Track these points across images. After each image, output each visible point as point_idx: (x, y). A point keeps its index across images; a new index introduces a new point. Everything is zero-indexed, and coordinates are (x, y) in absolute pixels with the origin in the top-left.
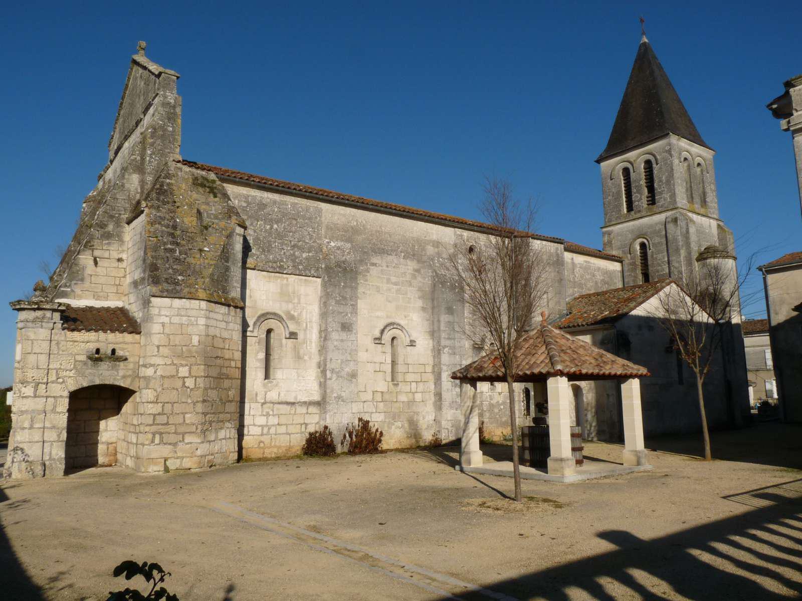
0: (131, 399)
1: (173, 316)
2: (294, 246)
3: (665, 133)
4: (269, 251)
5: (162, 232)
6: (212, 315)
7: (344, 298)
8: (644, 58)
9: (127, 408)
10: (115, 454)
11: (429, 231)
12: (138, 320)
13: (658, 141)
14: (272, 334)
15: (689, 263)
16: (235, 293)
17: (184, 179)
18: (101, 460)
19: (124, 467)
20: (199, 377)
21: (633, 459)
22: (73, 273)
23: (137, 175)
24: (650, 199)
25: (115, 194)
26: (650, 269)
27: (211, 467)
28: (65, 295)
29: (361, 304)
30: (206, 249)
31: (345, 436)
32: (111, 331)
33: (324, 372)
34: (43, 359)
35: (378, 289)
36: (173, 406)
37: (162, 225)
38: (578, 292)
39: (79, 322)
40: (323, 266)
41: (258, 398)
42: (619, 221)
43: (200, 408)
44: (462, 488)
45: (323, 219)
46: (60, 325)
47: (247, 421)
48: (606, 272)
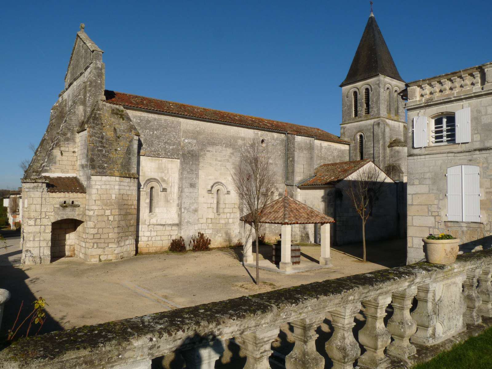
0: (81, 225)
1: (102, 185)
2: (166, 143)
3: (377, 74)
5: (96, 141)
6: (122, 183)
7: (192, 170)
8: (371, 25)
9: (80, 228)
10: (74, 250)
11: (240, 132)
12: (85, 186)
13: (373, 78)
14: (154, 189)
15: (384, 149)
16: (134, 171)
17: (107, 110)
18: (67, 253)
19: (78, 257)
20: (115, 215)
21: (324, 262)
22: (51, 159)
23: (82, 107)
24: (367, 110)
25: (71, 117)
26: (364, 150)
27: (122, 259)
28: (46, 171)
29: (201, 173)
30: (119, 149)
31: (191, 242)
32: (71, 192)
33: (180, 209)
34: (38, 207)
35: (210, 164)
36: (103, 230)
37: (96, 137)
38: (323, 162)
39: (55, 187)
40: (181, 153)
41: (146, 222)
42: (350, 122)
43: (116, 230)
44: (237, 276)
45: (182, 127)
46: (46, 190)
47: (141, 234)
48: (340, 151)
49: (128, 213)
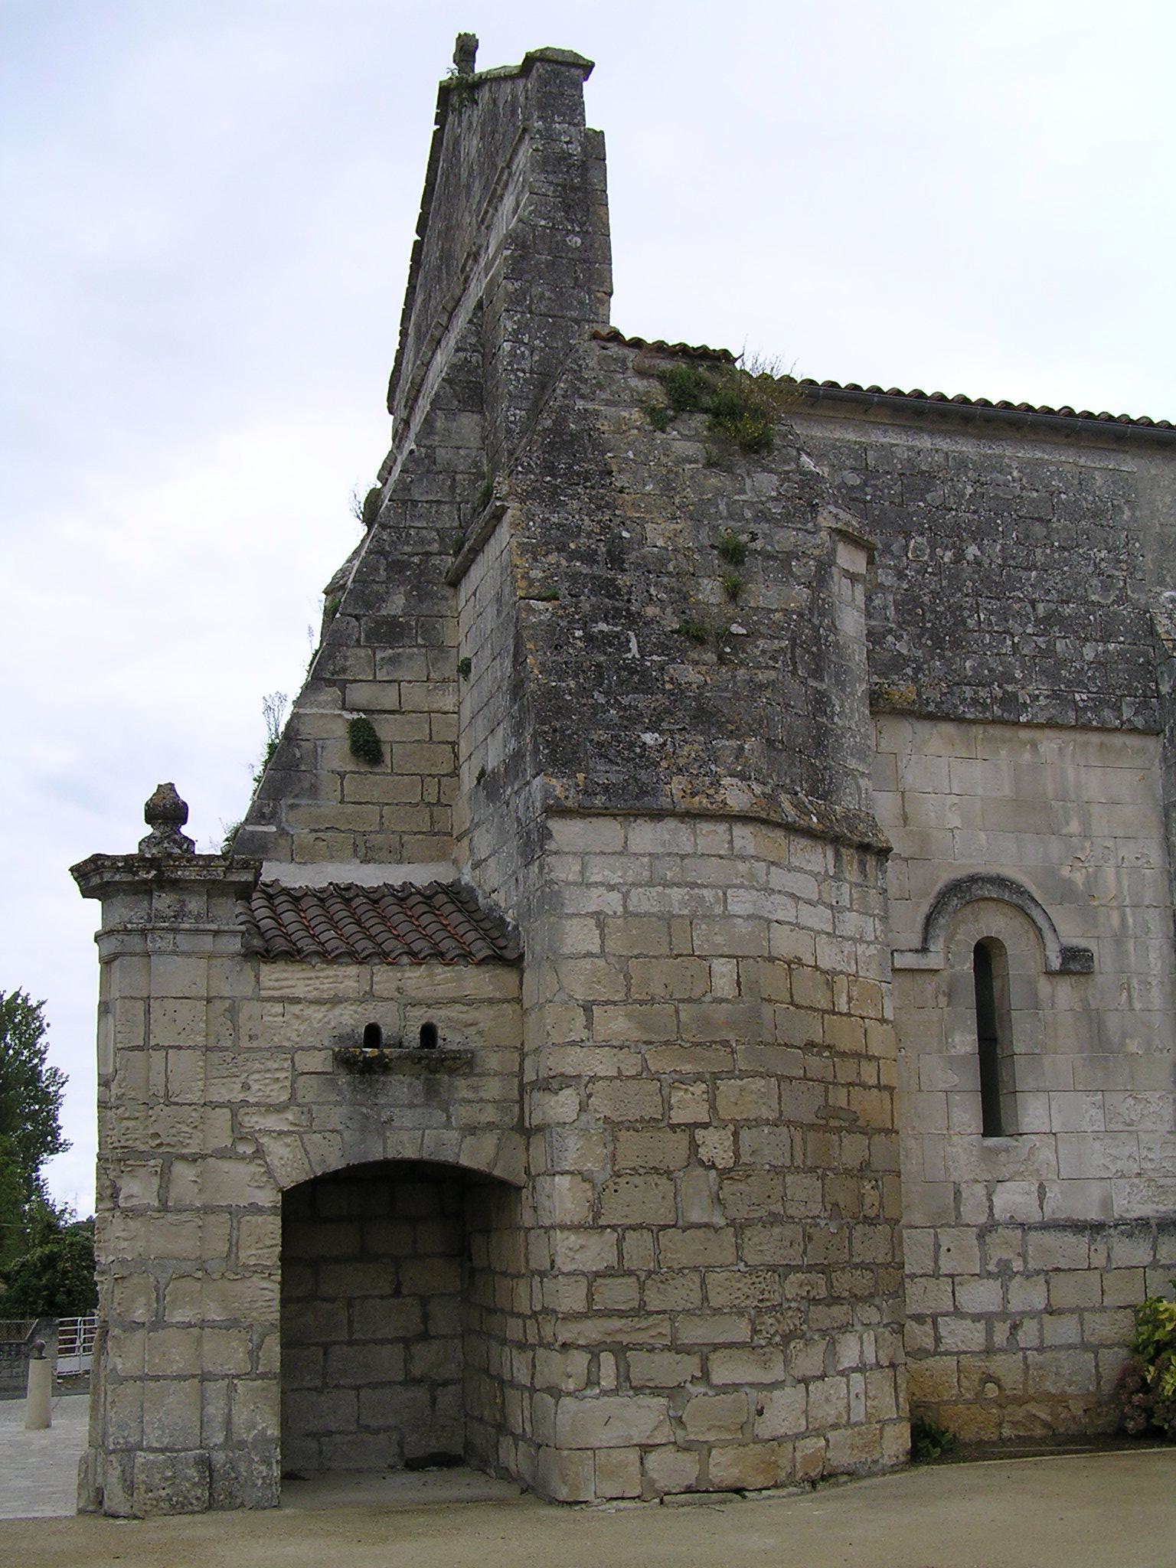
2: (1048, 620)
4: (956, 644)
5: (574, 577)
37: (572, 556)
49: (835, 1112)
